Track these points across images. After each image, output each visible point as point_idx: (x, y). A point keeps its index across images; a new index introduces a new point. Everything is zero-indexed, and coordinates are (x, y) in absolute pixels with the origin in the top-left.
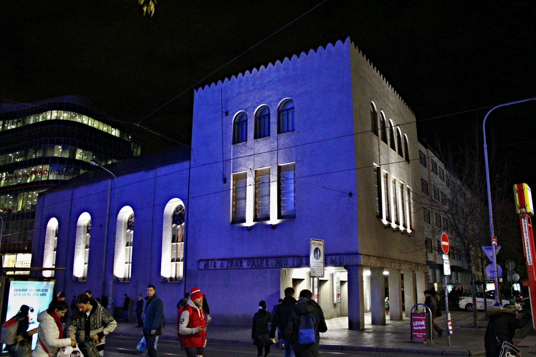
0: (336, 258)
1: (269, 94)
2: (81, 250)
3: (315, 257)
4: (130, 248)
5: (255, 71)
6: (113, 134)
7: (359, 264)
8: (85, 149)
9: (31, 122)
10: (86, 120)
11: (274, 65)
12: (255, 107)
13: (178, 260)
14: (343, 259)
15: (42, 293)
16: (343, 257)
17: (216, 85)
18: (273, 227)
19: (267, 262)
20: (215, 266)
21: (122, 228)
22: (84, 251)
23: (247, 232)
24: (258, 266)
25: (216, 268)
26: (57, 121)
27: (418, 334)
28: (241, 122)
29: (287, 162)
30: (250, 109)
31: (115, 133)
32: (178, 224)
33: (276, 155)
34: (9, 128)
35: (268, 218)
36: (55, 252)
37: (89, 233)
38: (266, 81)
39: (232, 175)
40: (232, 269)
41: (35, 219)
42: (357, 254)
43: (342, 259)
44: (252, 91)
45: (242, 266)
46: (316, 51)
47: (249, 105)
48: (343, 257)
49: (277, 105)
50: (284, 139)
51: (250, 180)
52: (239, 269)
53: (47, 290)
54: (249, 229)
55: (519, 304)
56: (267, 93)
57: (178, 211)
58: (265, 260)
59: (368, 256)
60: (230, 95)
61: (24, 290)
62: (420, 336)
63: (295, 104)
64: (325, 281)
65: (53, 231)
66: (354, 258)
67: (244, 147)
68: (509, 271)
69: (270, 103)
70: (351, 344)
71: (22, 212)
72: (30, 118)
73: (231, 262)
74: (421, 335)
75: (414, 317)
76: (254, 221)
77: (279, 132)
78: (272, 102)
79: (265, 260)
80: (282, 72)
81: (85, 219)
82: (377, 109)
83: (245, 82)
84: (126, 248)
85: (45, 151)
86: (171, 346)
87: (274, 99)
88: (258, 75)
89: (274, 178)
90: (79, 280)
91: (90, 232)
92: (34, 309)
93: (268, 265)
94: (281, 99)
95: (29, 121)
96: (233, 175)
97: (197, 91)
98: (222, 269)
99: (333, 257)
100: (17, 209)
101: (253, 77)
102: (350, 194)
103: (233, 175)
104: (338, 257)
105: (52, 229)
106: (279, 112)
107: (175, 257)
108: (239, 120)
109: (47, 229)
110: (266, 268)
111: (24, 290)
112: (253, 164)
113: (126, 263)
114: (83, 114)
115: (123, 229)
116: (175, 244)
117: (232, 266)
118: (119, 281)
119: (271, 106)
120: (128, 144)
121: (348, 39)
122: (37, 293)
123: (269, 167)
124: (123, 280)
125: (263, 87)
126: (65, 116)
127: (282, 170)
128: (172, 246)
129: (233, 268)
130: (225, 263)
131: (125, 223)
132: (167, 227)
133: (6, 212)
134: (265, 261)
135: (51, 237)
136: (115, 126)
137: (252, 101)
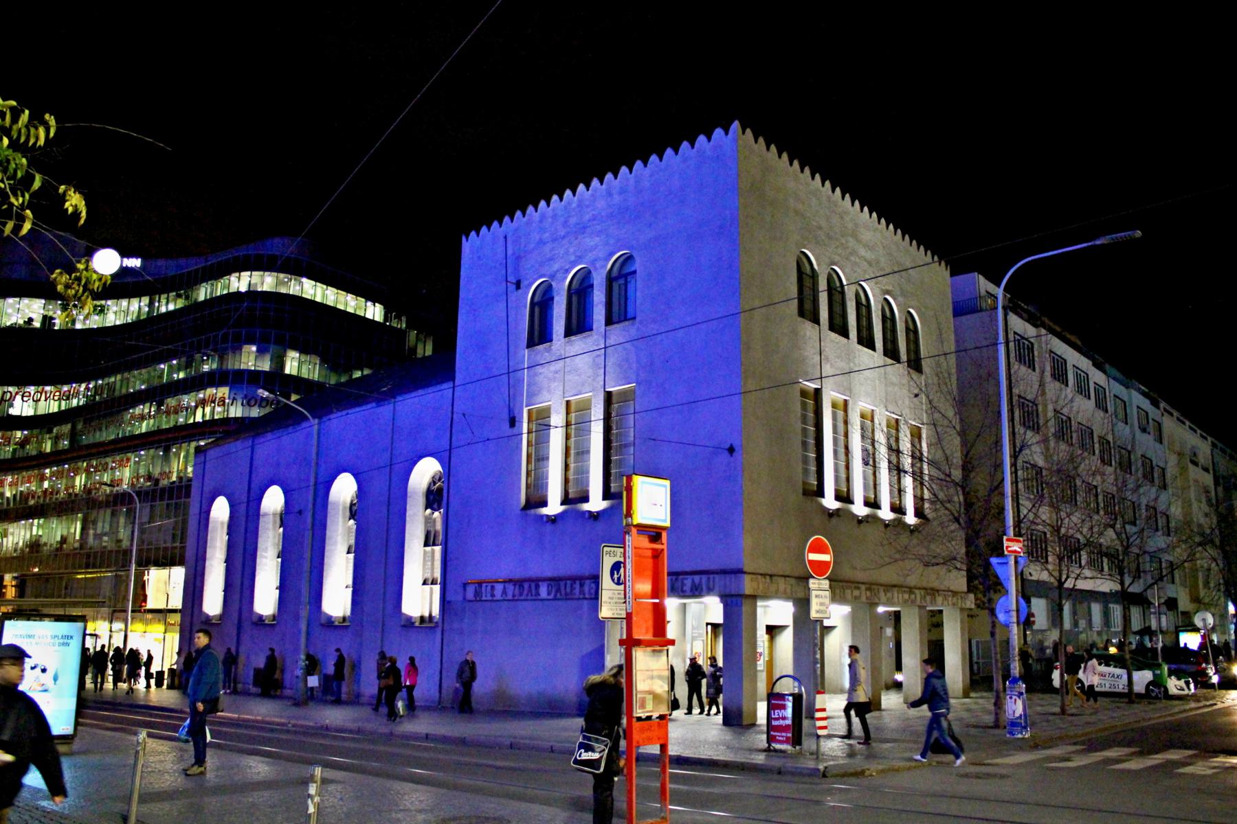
0: (701, 579)
1: (592, 243)
2: (268, 560)
3: (613, 580)
4: (433, 551)
5: (568, 196)
6: (369, 316)
7: (741, 593)
8: (303, 350)
9: (202, 298)
10: (311, 290)
11: (602, 184)
12: (567, 271)
13: (434, 582)
14: (714, 581)
15: (62, 641)
16: (714, 578)
17: (501, 226)
18: (595, 516)
19: (582, 585)
20: (493, 595)
21: (338, 518)
22: (422, 553)
23: (549, 527)
24: (566, 594)
25: (495, 599)
26: (252, 295)
27: (779, 734)
28: (543, 303)
29: (623, 382)
30: (559, 275)
31: (375, 312)
32: (434, 510)
33: (603, 370)
34: (163, 310)
35: (586, 499)
36: (280, 560)
37: (355, 520)
38: (587, 217)
39: (525, 411)
40: (521, 600)
41: (190, 500)
42: (740, 572)
43: (711, 583)
44: (563, 238)
45: (539, 595)
46: (677, 153)
47: (556, 266)
48: (714, 578)
49: (605, 266)
50: (618, 333)
51: (557, 419)
52: (534, 600)
53: (71, 637)
54: (553, 520)
55: (1183, 680)
56: (590, 242)
57: (435, 483)
58: (578, 582)
59: (768, 577)
60: (525, 246)
61: (30, 636)
62: (781, 738)
63: (638, 265)
64: (831, 628)
65: (222, 523)
66: (733, 580)
67: (547, 354)
68: (1155, 607)
69: (593, 262)
70: (739, 756)
71: (177, 484)
72: (199, 289)
73: (521, 586)
74: (783, 737)
75: (773, 702)
76: (562, 504)
77: (609, 321)
78: (596, 260)
79: (578, 582)
80: (617, 199)
81: (344, 488)
82: (818, 265)
83: (550, 220)
84: (347, 557)
85: (222, 359)
86: (346, 744)
87: (601, 255)
88: (574, 205)
89: (597, 412)
90: (264, 621)
91: (356, 517)
92: (47, 667)
93: (584, 594)
94: (615, 253)
95: (198, 294)
96: (529, 410)
97: (467, 241)
98: (492, 601)
99: (697, 578)
100: (169, 478)
101: (565, 208)
102: (731, 450)
103: (529, 410)
104: (704, 578)
105: (220, 519)
106: (610, 280)
107: (428, 575)
108: (581, 284)
109: (211, 520)
110: (579, 599)
111: (30, 636)
112: (561, 388)
113: (347, 587)
114: (302, 276)
115: (341, 519)
116: (428, 549)
117: (521, 594)
118: (413, 623)
119: (596, 269)
120: (401, 334)
121: (736, 125)
122: (52, 641)
123: (591, 394)
124: (341, 620)
125: (582, 229)
126: (267, 282)
127: (614, 399)
128: (425, 552)
129: (522, 598)
130: (510, 587)
131: (344, 508)
132: (415, 514)
133: (149, 484)
134: (577, 585)
135: (219, 536)
136: (372, 297)
137: (563, 257)
